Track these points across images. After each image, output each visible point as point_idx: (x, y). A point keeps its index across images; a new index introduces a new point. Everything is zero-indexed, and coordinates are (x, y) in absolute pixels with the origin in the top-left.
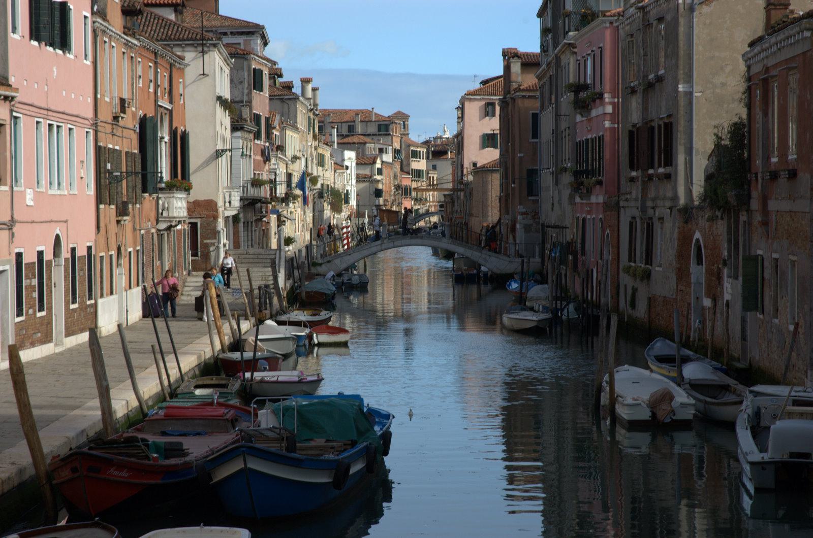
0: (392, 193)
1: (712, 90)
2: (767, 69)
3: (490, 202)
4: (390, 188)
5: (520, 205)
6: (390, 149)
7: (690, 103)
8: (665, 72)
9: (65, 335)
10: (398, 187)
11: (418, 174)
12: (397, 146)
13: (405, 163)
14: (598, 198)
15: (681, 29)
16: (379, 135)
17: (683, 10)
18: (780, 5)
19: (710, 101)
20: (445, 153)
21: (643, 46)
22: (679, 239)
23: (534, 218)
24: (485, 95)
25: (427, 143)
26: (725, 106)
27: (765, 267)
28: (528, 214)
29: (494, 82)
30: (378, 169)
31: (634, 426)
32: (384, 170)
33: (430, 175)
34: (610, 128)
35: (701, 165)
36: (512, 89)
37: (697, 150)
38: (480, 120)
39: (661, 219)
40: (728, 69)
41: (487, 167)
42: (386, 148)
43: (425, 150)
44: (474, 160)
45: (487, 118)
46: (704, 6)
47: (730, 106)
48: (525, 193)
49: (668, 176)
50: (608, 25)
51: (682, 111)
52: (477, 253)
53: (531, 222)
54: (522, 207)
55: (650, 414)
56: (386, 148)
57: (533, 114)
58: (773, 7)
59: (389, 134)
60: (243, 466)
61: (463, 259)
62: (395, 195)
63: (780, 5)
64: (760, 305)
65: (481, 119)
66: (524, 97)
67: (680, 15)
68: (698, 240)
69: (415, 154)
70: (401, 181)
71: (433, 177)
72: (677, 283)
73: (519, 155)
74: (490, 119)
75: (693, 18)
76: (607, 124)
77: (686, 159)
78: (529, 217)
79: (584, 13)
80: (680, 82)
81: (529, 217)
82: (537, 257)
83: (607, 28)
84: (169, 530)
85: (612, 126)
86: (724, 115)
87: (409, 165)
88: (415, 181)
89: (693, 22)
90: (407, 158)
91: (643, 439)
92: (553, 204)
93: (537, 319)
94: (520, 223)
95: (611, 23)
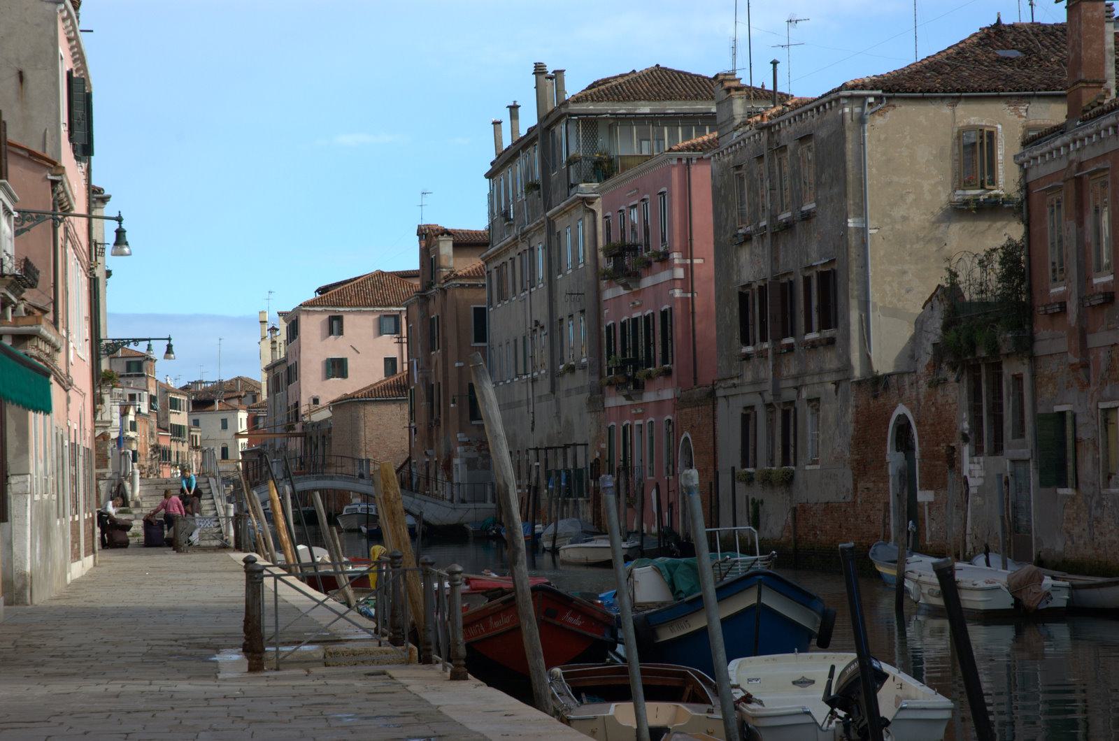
0: (149, 456)
1: (891, 226)
2: (1081, 166)
3: (363, 445)
4: (146, 450)
5: (460, 432)
6: (145, 395)
7: (864, 244)
8: (817, 206)
9: (85, 553)
10: (156, 448)
11: (177, 431)
12: (153, 391)
13: (161, 416)
14: (661, 393)
15: (850, 147)
16: (128, 376)
17: (850, 121)
18: (1094, 82)
19: (890, 240)
20: (212, 403)
21: (769, 177)
22: (857, 422)
23: (479, 449)
24: (328, 306)
25: (185, 389)
26: (908, 246)
27: (1077, 424)
28: (471, 444)
29: (336, 290)
30: (131, 422)
31: (990, 617)
32: (138, 424)
33: (192, 433)
34: (682, 298)
35: (59, 568)
36: (442, 277)
37: (875, 304)
38: (322, 340)
39: (814, 402)
40: (910, 198)
41: (358, 398)
42: (140, 394)
43: (186, 399)
44: (315, 394)
45: (332, 337)
46: (877, 117)
47: (914, 246)
48: (467, 415)
49: (831, 342)
50: (675, 162)
51: (853, 253)
52: (408, 498)
53: (476, 455)
54: (463, 435)
55: (1012, 601)
56: (140, 394)
57: (475, 308)
58: (1084, 85)
59: (143, 375)
60: (755, 602)
61: (356, 516)
62: (152, 459)
63: (1094, 82)
64: (1070, 475)
65: (324, 338)
66: (462, 286)
67: (846, 128)
68: (902, 417)
69: (175, 404)
70: (158, 440)
71: (196, 436)
72: (854, 480)
73: (457, 365)
74: (336, 339)
75: (864, 132)
76: (678, 293)
77: (861, 316)
78: (473, 448)
79: (599, 158)
80: (849, 216)
81: (473, 448)
82: (489, 501)
83: (673, 166)
84: (753, 657)
85: (685, 295)
86: (908, 258)
87: (167, 418)
88: (174, 440)
89: (864, 136)
90: (164, 408)
91: (1004, 635)
92: (533, 422)
93: (628, 546)
94: (461, 457)
95: (680, 159)
